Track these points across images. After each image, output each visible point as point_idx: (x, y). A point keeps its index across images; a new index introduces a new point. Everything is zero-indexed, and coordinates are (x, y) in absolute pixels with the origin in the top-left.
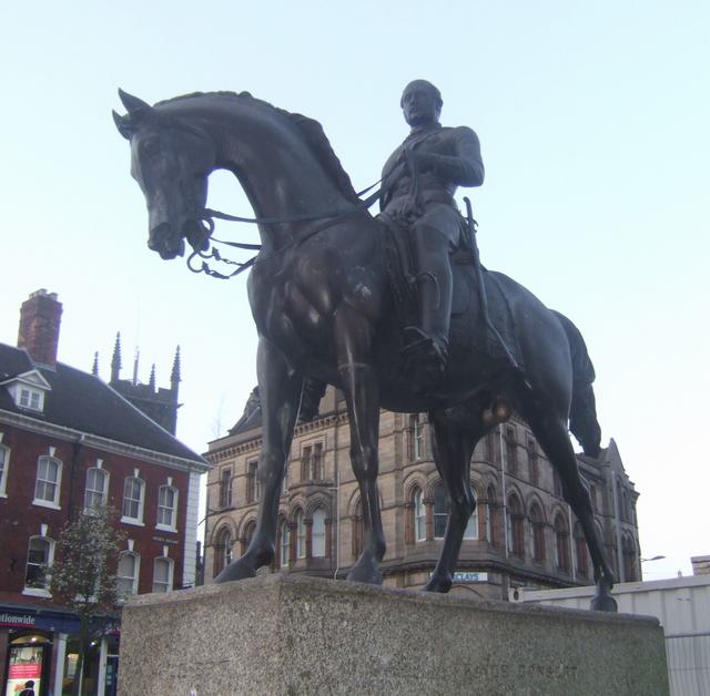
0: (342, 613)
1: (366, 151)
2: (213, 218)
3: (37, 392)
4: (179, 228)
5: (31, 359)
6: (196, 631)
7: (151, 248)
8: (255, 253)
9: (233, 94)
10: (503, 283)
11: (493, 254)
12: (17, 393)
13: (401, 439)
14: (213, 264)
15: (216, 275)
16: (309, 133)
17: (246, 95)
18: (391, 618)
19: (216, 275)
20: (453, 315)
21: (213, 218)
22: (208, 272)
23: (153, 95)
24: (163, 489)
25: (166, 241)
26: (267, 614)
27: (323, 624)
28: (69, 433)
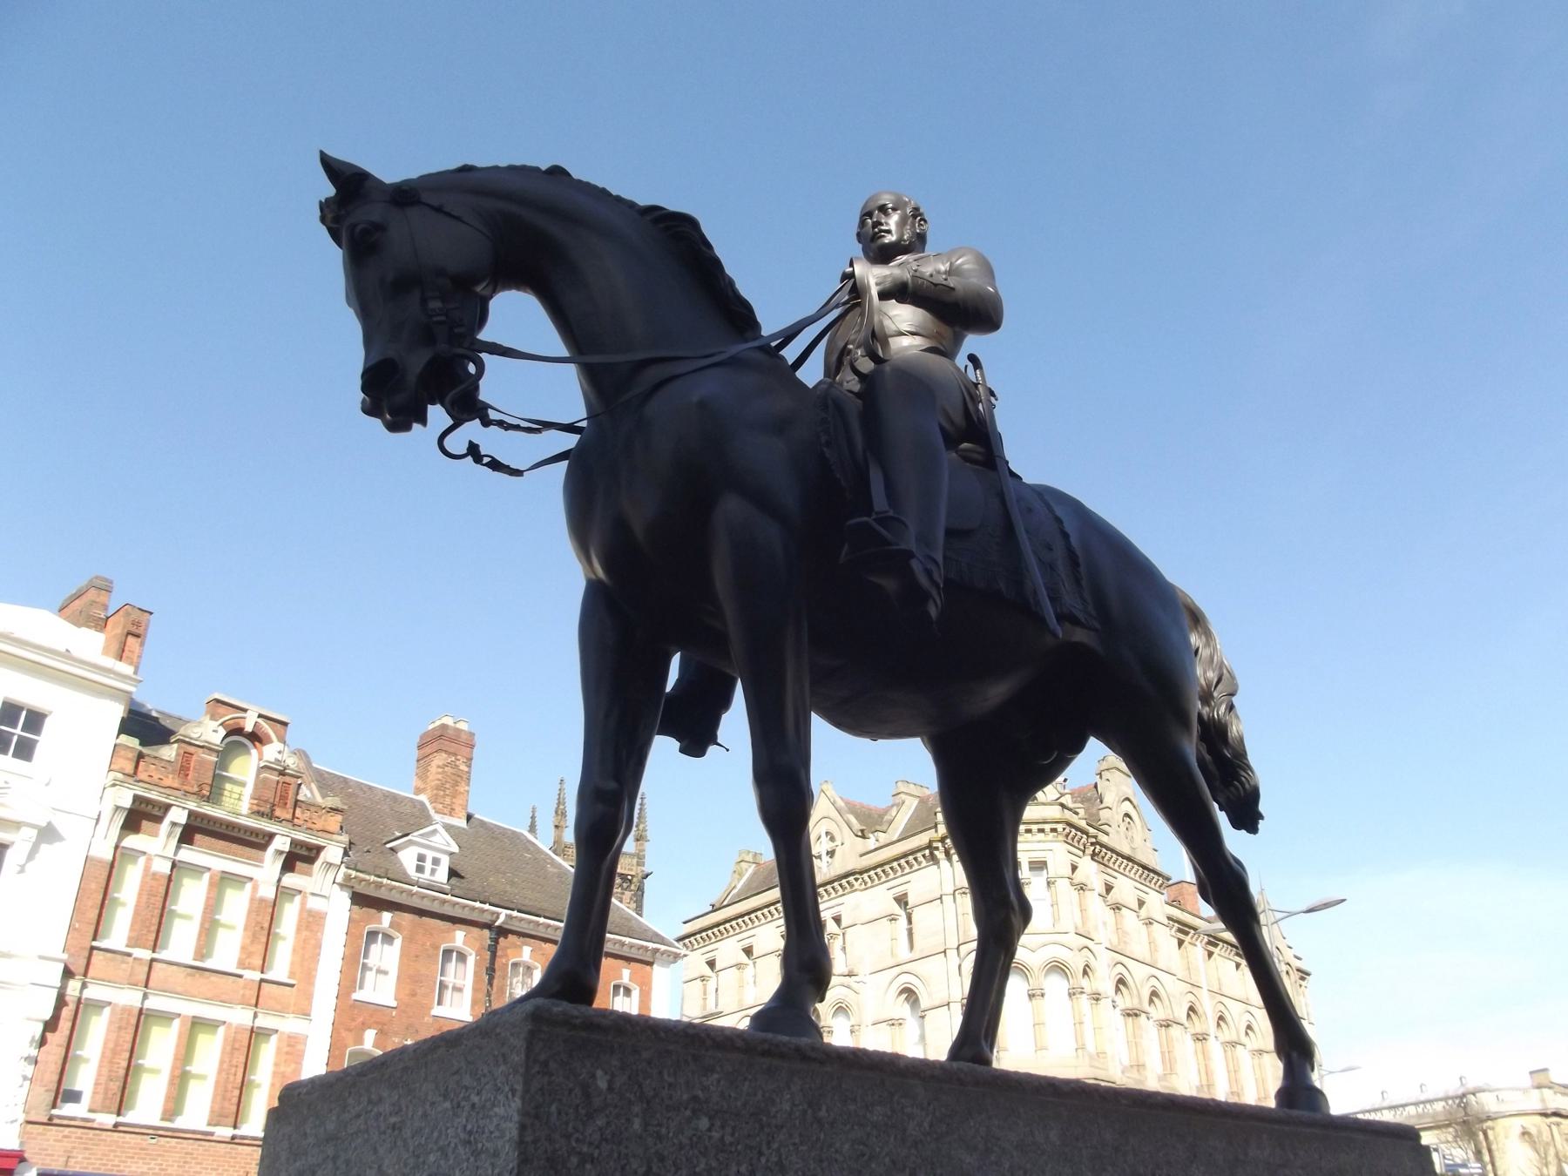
0: (695, 1098)
1: (783, 277)
2: (484, 356)
3: (438, 855)
4: (419, 373)
5: (432, 812)
6: (375, 1151)
7: (371, 409)
8: (570, 441)
9: (537, 169)
10: (1047, 496)
11: (1034, 453)
12: (408, 858)
13: (872, 780)
14: (492, 441)
15: (495, 465)
16: (678, 239)
17: (557, 172)
18: (823, 1113)
19: (495, 465)
20: (950, 533)
21: (484, 356)
22: (478, 458)
23: (391, 166)
24: (617, 987)
25: (393, 395)
26: (501, 1097)
27: (646, 1125)
28: (483, 911)
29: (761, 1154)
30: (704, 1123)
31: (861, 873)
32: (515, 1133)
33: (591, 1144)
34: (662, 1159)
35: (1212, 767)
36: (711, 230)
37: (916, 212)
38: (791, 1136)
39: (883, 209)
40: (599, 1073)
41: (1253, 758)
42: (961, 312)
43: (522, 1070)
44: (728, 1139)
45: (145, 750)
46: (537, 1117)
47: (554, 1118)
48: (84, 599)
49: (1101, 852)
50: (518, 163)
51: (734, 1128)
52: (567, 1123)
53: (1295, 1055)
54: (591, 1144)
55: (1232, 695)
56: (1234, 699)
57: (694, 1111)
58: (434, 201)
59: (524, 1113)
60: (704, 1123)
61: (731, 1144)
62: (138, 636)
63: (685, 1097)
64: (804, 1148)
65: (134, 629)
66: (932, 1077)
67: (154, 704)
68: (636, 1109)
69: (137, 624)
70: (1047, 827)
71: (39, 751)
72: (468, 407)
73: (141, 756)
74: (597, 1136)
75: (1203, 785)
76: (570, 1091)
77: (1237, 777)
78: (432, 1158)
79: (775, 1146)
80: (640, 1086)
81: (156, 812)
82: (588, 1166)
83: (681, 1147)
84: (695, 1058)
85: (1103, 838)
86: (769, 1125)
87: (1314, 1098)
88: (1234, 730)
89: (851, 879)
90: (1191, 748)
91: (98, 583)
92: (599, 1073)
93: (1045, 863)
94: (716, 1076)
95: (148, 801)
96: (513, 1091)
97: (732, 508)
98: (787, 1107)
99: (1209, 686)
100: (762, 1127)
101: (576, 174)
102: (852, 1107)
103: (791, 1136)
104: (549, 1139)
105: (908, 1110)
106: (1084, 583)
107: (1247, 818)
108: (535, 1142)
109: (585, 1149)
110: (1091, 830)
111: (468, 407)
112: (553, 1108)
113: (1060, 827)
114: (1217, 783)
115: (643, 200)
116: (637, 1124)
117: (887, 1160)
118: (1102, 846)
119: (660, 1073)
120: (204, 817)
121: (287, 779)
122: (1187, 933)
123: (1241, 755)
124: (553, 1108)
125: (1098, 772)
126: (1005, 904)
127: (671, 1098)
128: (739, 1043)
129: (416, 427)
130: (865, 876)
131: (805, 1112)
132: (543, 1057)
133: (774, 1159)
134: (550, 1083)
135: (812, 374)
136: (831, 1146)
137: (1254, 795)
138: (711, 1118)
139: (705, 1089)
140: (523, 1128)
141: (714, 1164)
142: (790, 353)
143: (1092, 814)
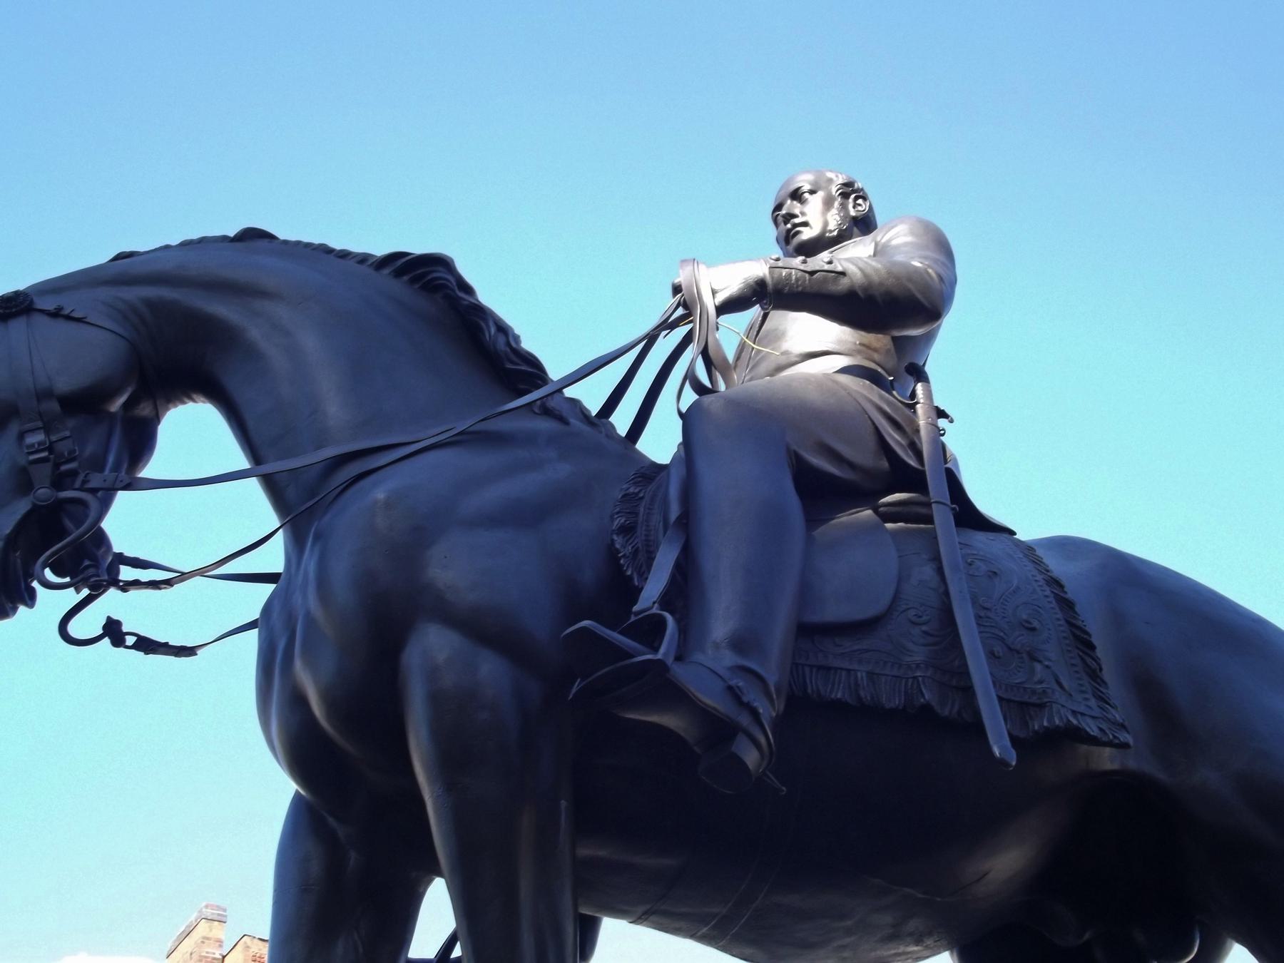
1: (570, 311)
15: (146, 645)
17: (252, 235)
19: (146, 645)
36: (467, 270)
37: (848, 190)
39: (797, 195)
42: (896, 314)
48: (197, 935)
50: (195, 235)
58: (49, 304)
72: (94, 567)
91: (209, 912)
97: (432, 647)
101: (282, 235)
106: (1108, 674)
111: (94, 567)
115: (380, 249)
129: (22, 609)
135: (661, 443)
142: (622, 420)
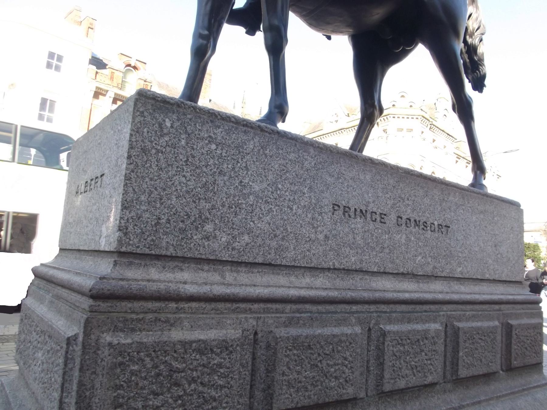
0: (210, 137)
18: (267, 152)
29: (238, 162)
30: (213, 147)
31: (346, 129)
32: (128, 137)
33: (161, 146)
34: (194, 157)
35: (468, 64)
38: (252, 158)
40: (167, 120)
41: (486, 62)
43: (132, 114)
44: (224, 154)
45: (98, 71)
46: (137, 132)
47: (145, 134)
49: (432, 127)
51: (227, 151)
52: (151, 137)
53: (478, 172)
54: (161, 146)
55: (483, 34)
56: (483, 37)
57: (209, 141)
59: (132, 130)
60: (213, 147)
61: (225, 156)
62: (92, 29)
63: (206, 135)
64: (258, 163)
65: (91, 26)
66: (318, 147)
67: (100, 56)
68: (183, 136)
69: (91, 24)
70: (415, 117)
71: (62, 69)
73: (97, 73)
74: (165, 144)
75: (462, 70)
76: (153, 125)
77: (478, 69)
78: (107, 152)
79: (245, 160)
80: (186, 128)
81: (103, 92)
82: (160, 154)
83: (203, 154)
84: (212, 121)
85: (434, 123)
86: (243, 152)
87: (482, 186)
88: (480, 50)
89: (343, 131)
90: (459, 46)
92: (167, 120)
93: (412, 130)
94: (220, 130)
95: (101, 89)
96: (129, 122)
98: (252, 147)
99: (473, 30)
100: (240, 152)
102: (281, 152)
103: (252, 158)
104: (142, 141)
105: (306, 157)
107: (479, 85)
108: (136, 141)
109: (159, 148)
110: (431, 120)
112: (145, 130)
113: (419, 117)
114: (469, 71)
116: (183, 142)
117: (294, 174)
118: (434, 125)
119: (195, 124)
120: (119, 95)
121: (147, 83)
122: (459, 159)
123: (481, 60)
124: (145, 130)
125: (420, 58)
126: (373, 106)
127: (199, 135)
128: (233, 119)
130: (348, 130)
131: (259, 150)
132: (141, 110)
133: (244, 165)
134: (144, 120)
136: (270, 164)
137: (483, 77)
138: (217, 145)
139: (214, 134)
140: (131, 135)
141: (217, 162)
143: (415, 74)
